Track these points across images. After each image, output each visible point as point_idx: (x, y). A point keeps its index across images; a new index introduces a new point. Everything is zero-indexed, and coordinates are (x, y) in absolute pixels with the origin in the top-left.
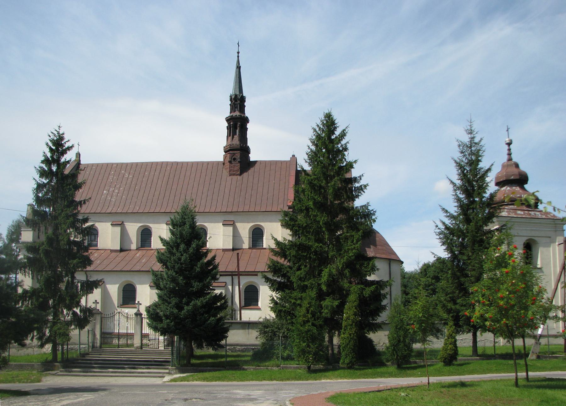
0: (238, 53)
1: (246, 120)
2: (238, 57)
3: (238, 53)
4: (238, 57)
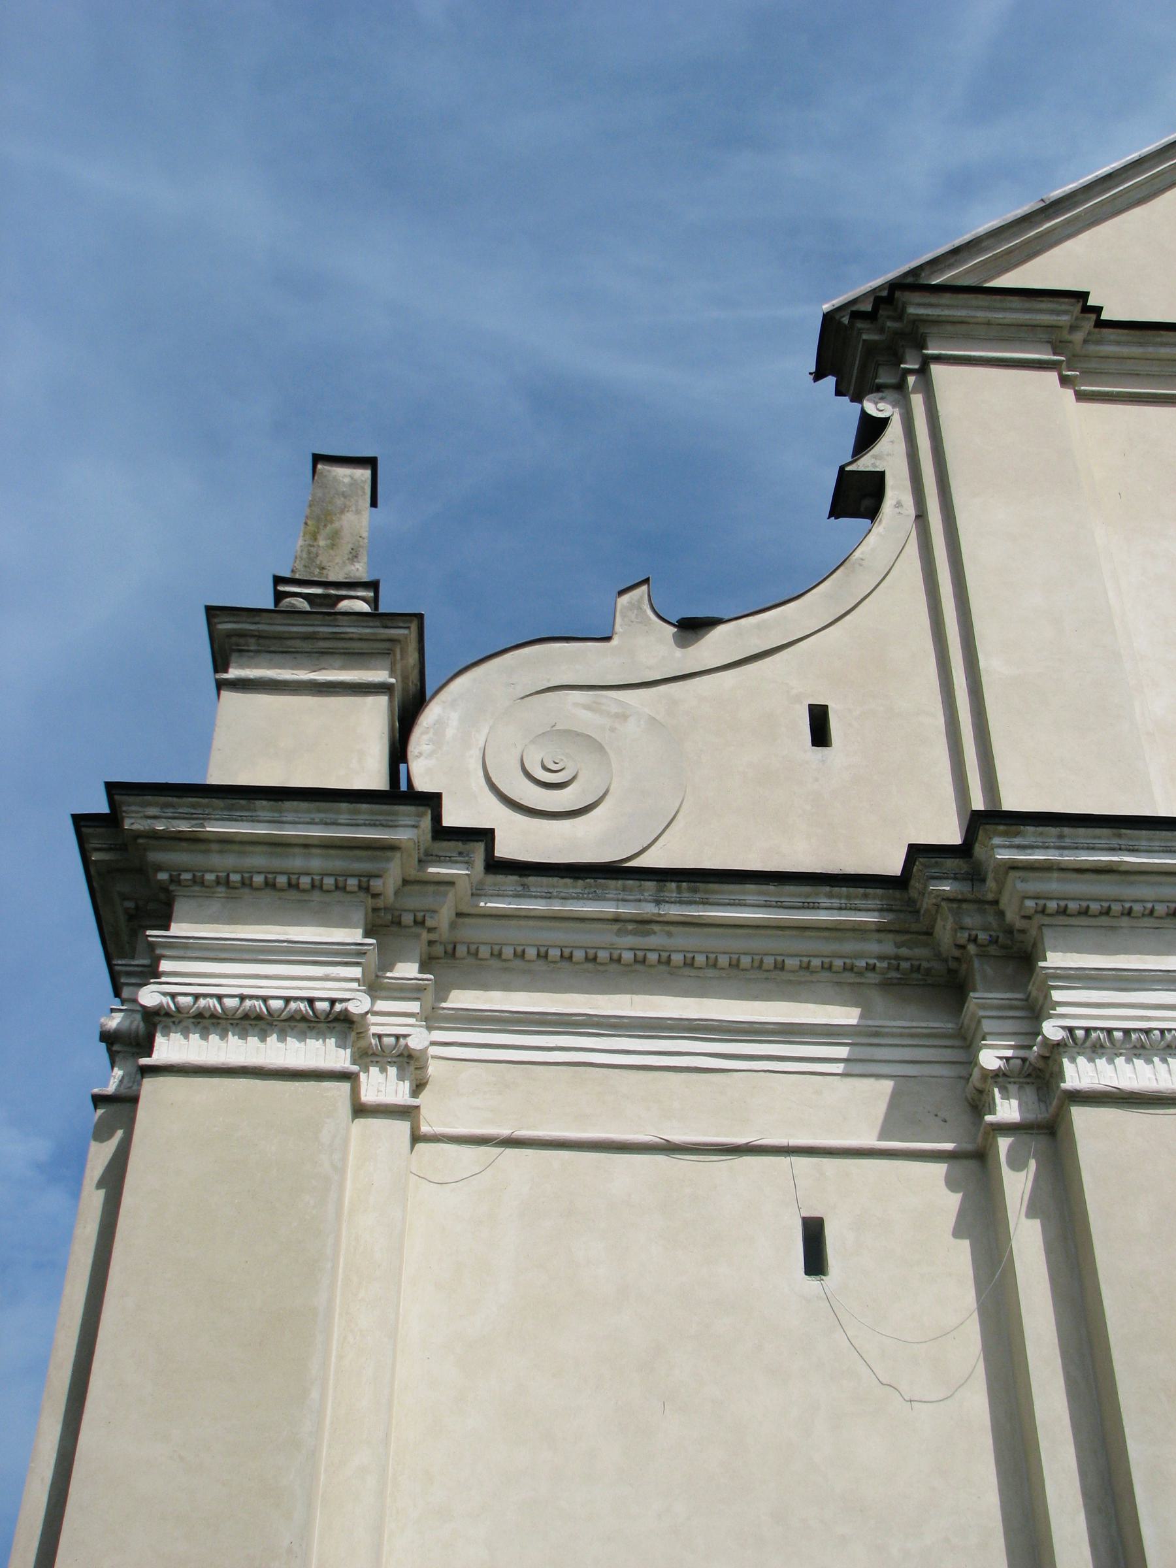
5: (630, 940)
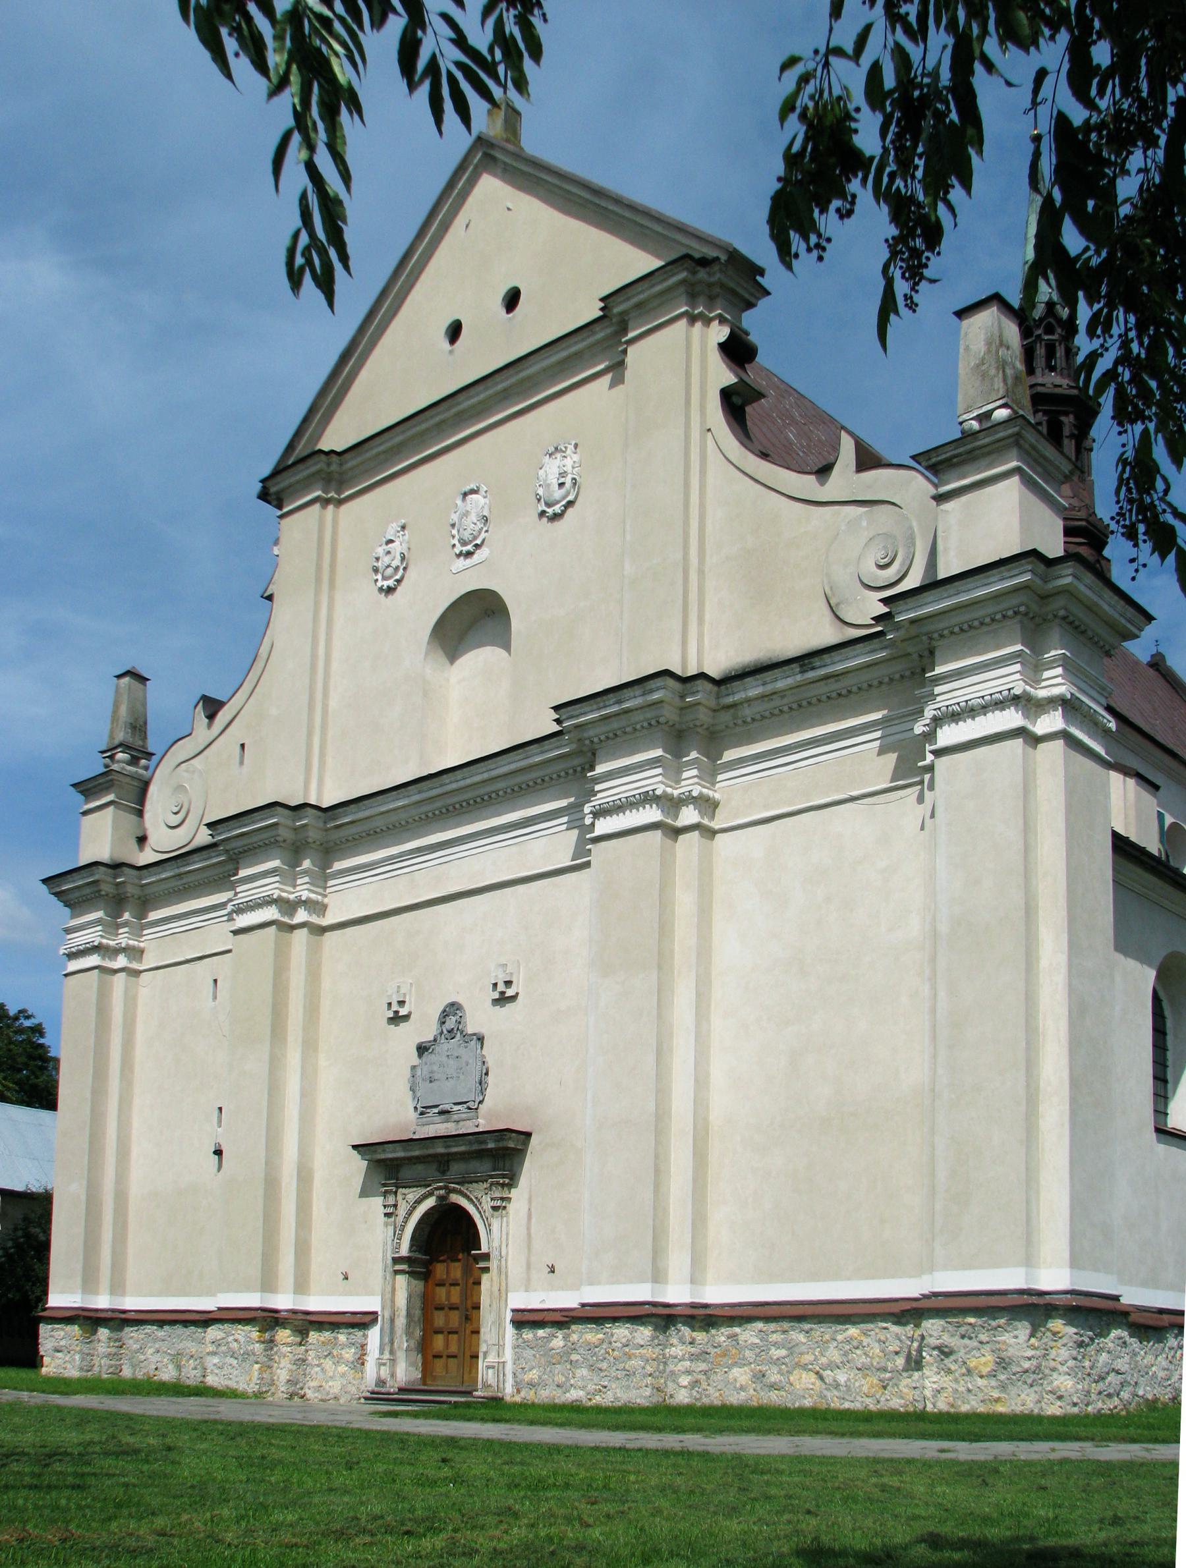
5: (179, 883)
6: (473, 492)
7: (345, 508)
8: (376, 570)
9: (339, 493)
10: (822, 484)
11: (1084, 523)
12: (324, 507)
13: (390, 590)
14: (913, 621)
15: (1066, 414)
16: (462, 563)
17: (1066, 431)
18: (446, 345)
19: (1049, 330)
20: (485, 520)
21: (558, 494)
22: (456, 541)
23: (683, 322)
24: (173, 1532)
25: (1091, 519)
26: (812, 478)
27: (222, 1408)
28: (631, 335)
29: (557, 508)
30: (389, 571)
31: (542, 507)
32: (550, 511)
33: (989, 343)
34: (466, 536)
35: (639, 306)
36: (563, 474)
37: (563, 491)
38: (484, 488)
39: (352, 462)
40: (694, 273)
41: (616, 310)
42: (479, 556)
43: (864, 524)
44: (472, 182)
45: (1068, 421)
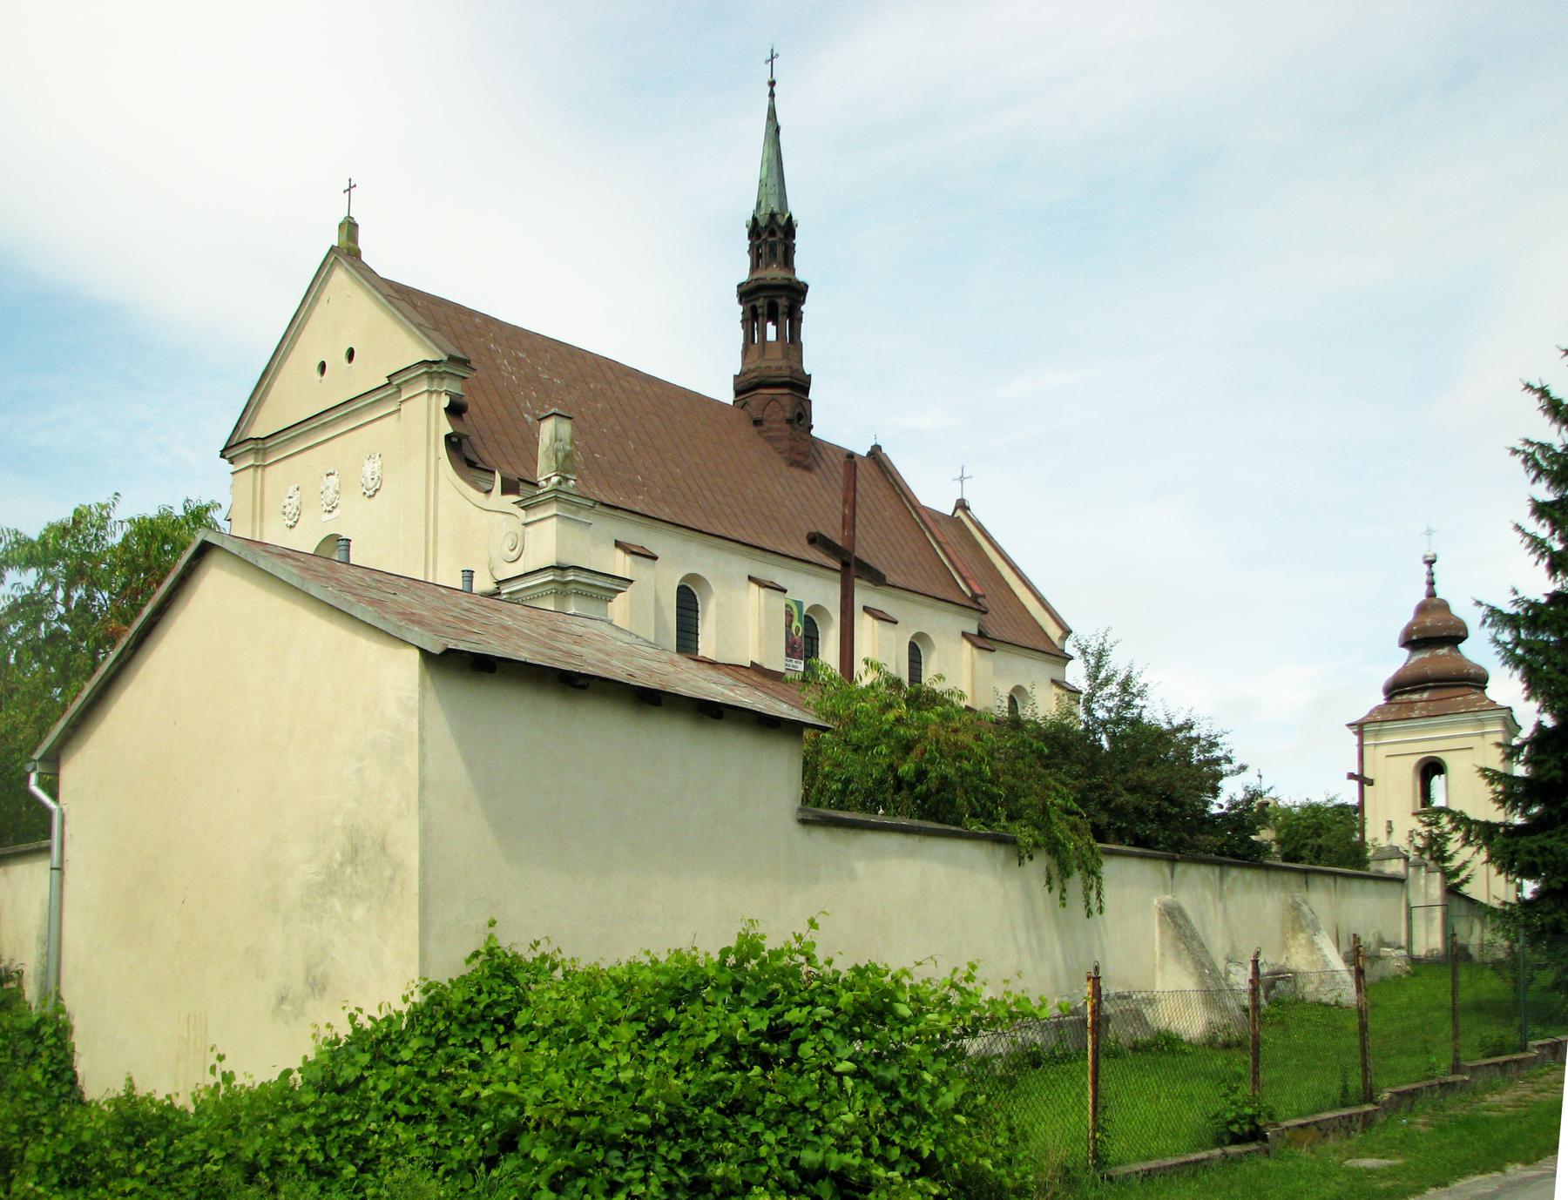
0: (772, 84)
1: (798, 292)
2: (772, 95)
3: (772, 84)
4: (772, 95)
6: (331, 474)
7: (267, 470)
8: (284, 514)
9: (264, 460)
10: (488, 498)
11: (787, 379)
12: (255, 471)
13: (291, 527)
14: (510, 593)
15: (781, 297)
16: (327, 516)
17: (781, 309)
18: (318, 376)
19: (772, 233)
20: (337, 492)
21: (371, 484)
22: (323, 502)
23: (426, 395)
24: (975, 1112)
25: (793, 375)
26: (483, 495)
27: (30, 987)
28: (403, 398)
29: (371, 492)
30: (291, 516)
31: (364, 490)
32: (368, 493)
33: (551, 440)
34: (329, 502)
35: (405, 382)
36: (373, 473)
37: (373, 483)
38: (337, 473)
39: (270, 443)
40: (431, 368)
41: (395, 383)
42: (336, 512)
43: (504, 525)
44: (330, 273)
45: (783, 303)
